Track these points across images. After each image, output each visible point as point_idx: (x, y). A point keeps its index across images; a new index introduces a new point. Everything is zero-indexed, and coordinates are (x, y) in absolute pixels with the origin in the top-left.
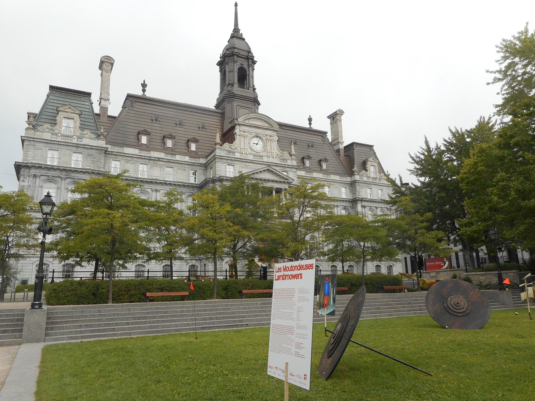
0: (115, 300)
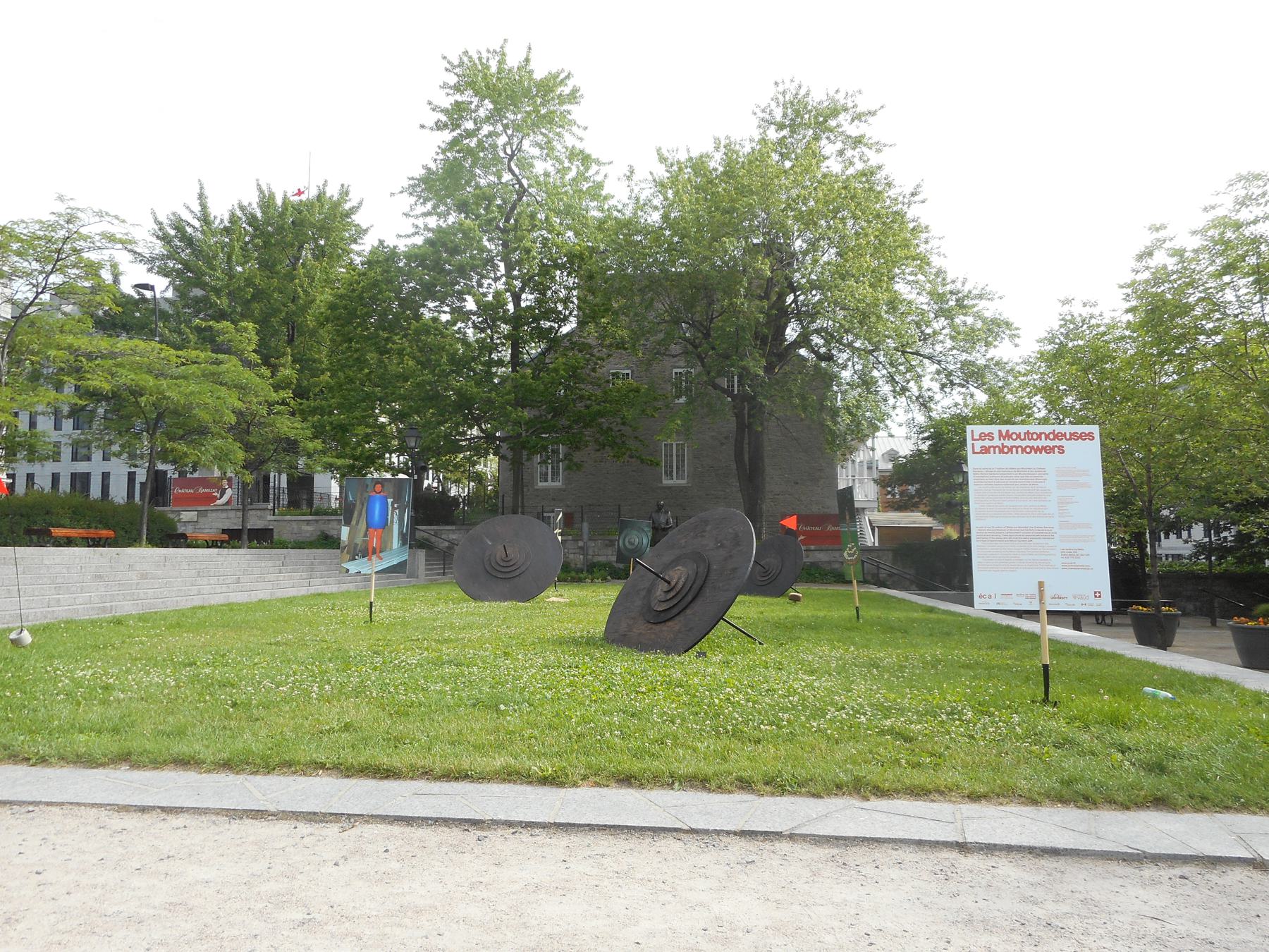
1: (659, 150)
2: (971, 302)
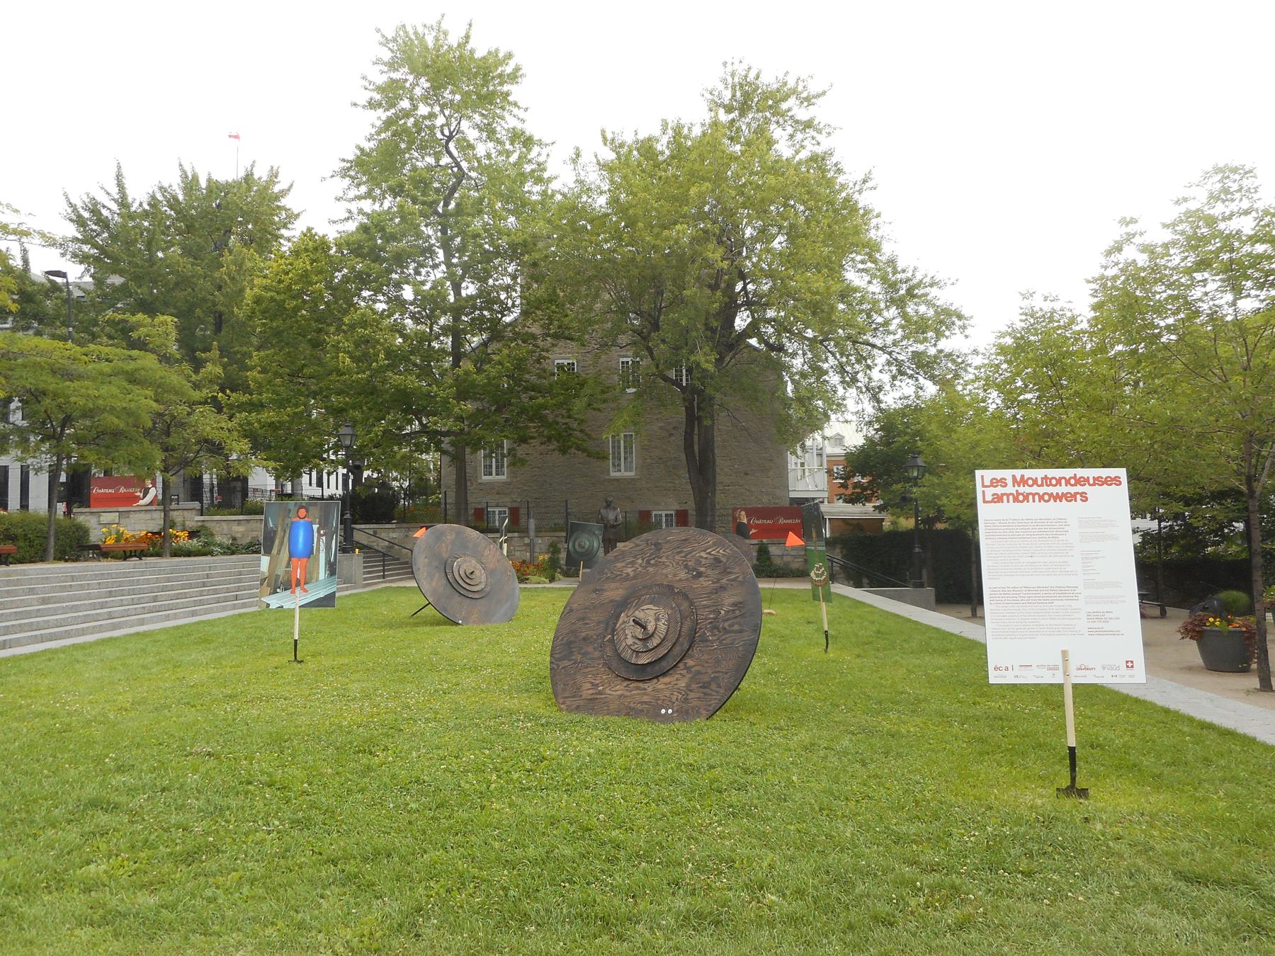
0: (62, 557)
1: (603, 133)
2: (922, 291)
